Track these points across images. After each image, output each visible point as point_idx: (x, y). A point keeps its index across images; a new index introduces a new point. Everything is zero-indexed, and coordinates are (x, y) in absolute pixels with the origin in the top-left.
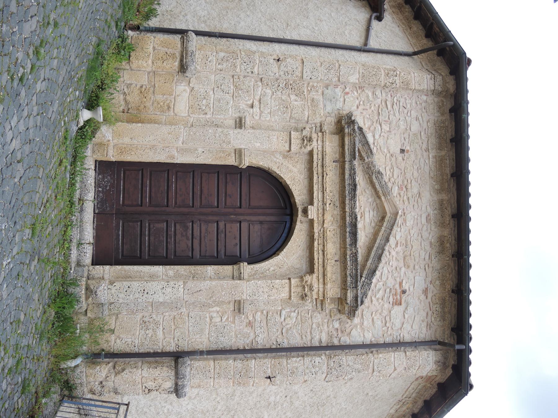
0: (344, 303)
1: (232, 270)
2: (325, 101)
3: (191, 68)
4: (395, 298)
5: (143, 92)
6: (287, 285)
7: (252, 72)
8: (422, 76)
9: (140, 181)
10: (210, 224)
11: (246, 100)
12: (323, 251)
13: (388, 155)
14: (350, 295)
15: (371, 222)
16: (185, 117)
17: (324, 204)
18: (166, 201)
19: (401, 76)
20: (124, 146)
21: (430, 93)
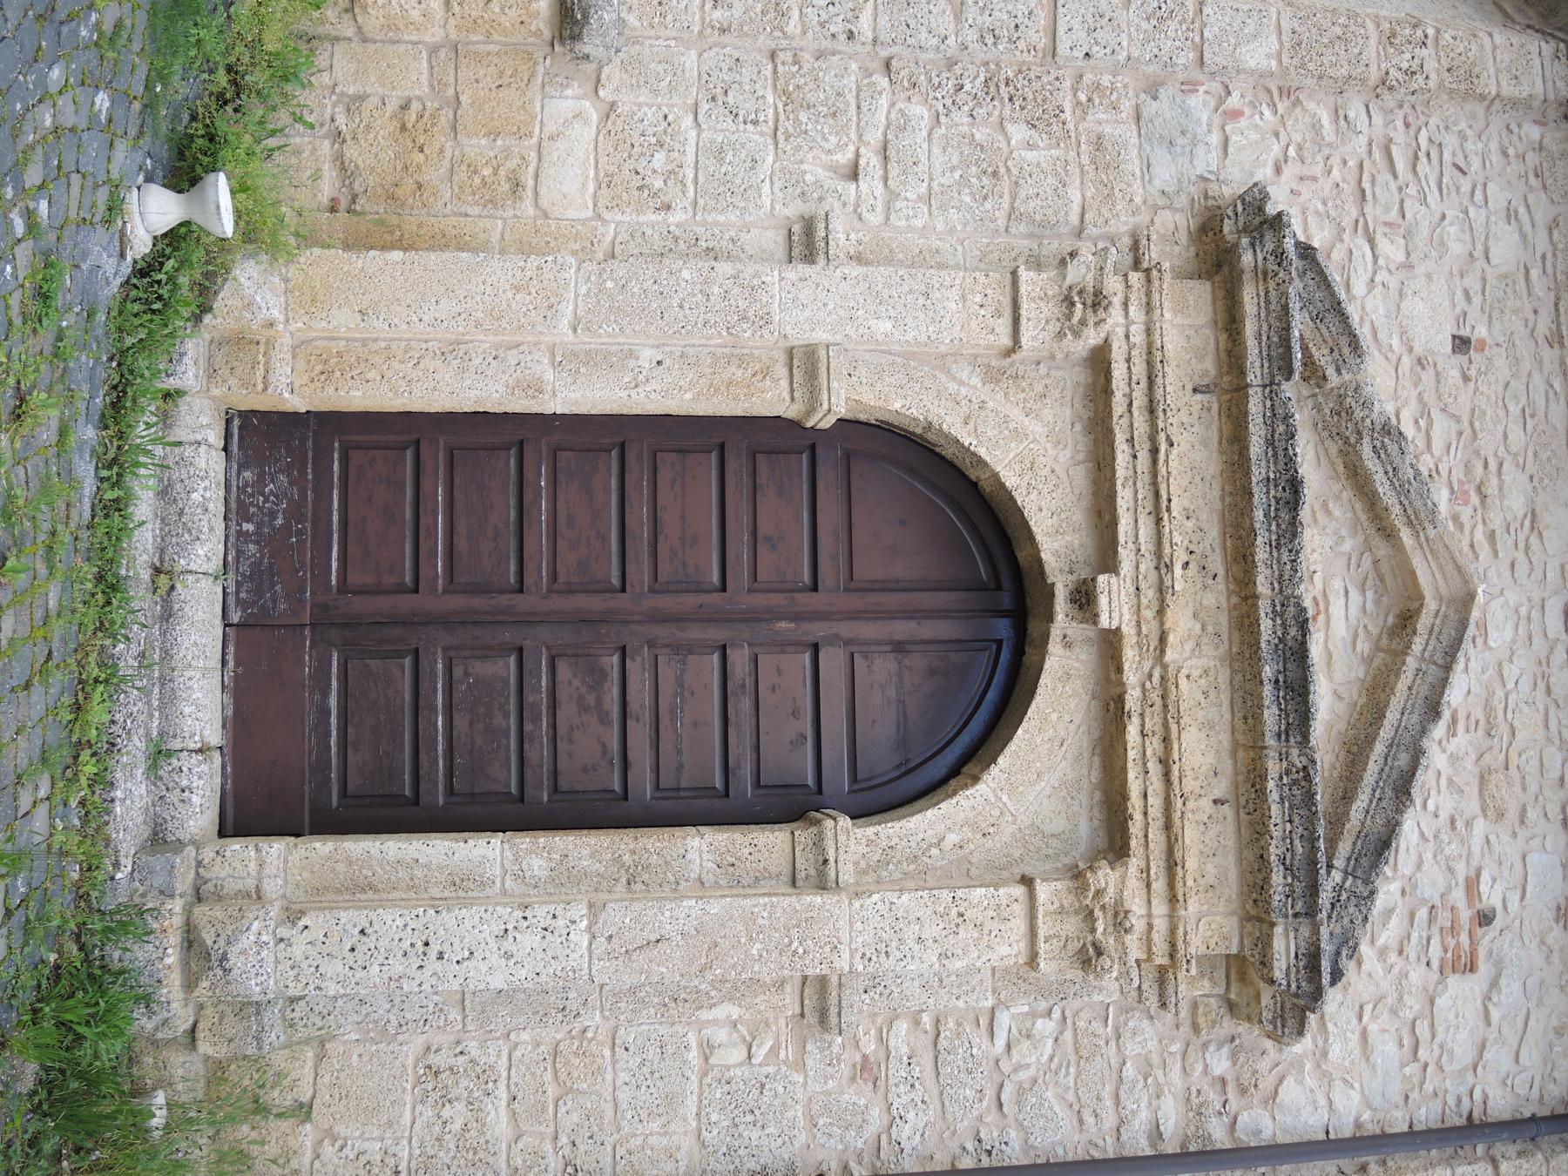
0: (1253, 975)
1: (788, 850)
2: (1147, 147)
3: (601, 17)
4: (1451, 942)
5: (409, 125)
6: (1019, 910)
7: (851, 36)
8: (1522, 46)
9: (409, 492)
10: (692, 659)
11: (827, 146)
12: (1165, 762)
13: (1406, 360)
14: (1284, 947)
15: (1356, 636)
16: (583, 222)
17: (1163, 565)
18: (513, 568)
19: (1443, 43)
20: (336, 347)
21: (1552, 114)
